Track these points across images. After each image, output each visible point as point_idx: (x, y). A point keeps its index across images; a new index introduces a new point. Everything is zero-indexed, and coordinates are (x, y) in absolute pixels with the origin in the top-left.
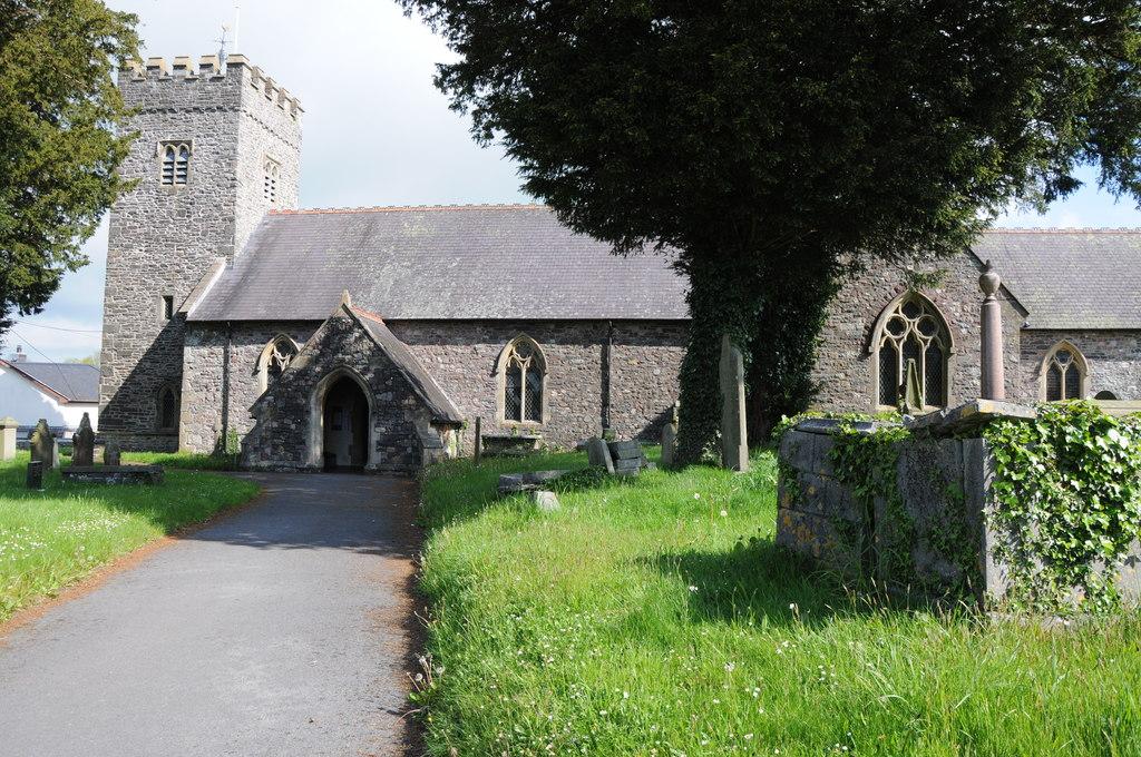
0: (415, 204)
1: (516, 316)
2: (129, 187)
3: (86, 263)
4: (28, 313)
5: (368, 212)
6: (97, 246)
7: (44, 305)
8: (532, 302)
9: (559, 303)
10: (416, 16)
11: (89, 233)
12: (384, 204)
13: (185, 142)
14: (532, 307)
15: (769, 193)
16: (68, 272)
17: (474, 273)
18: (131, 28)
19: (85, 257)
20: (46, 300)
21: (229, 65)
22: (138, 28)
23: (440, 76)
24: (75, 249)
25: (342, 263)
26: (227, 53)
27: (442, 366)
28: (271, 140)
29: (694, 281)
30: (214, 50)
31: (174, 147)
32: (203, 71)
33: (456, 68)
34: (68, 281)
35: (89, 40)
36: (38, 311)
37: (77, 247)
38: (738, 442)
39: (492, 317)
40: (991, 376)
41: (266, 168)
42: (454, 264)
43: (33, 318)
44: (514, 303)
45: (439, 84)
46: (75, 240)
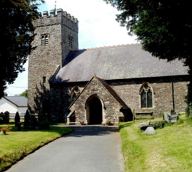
0: (112, 45)
1: (143, 77)
2: (34, 48)
3: (24, 70)
4: (11, 84)
5: (98, 49)
6: (26, 66)
7: (14, 82)
8: (148, 72)
9: (156, 72)
10: (110, 5)
11: (25, 62)
12: (103, 46)
13: (47, 34)
14: (148, 73)
15: (173, 79)
16: (20, 73)
17: (131, 64)
18: (36, 10)
19: (24, 68)
20: (14, 80)
21: (58, 12)
22: (37, 10)
23: (117, 18)
24: (21, 67)
25: (92, 64)
26: (57, 8)
27: (123, 93)
28: (70, 31)
29: (190, 68)
30: (53, 8)
31: (44, 36)
32: (51, 14)
33: (120, 15)
34: (20, 74)
35: (27, 18)
36: (13, 83)
37: (22, 66)
38: (99, 127)
39: (137, 77)
40: (65, 136)
41: (69, 39)
42: (125, 62)
43: (12, 85)
44: (143, 73)
45: (116, 20)
46: (21, 64)
